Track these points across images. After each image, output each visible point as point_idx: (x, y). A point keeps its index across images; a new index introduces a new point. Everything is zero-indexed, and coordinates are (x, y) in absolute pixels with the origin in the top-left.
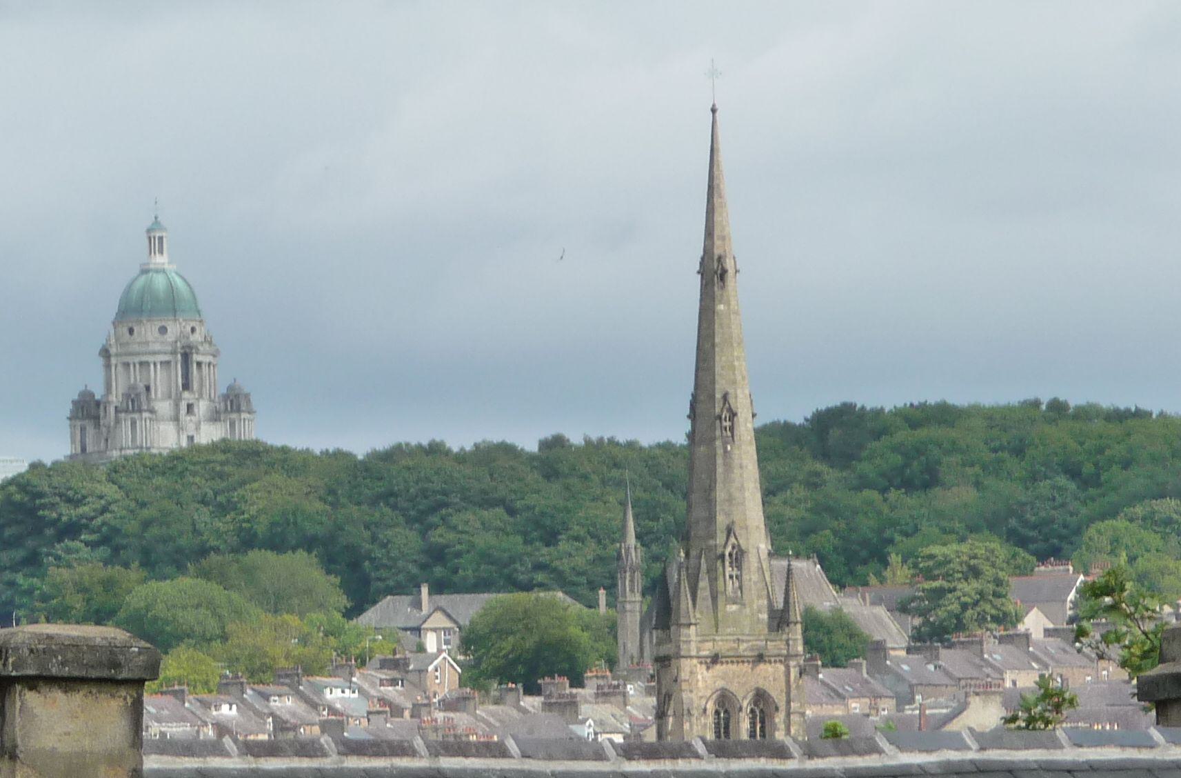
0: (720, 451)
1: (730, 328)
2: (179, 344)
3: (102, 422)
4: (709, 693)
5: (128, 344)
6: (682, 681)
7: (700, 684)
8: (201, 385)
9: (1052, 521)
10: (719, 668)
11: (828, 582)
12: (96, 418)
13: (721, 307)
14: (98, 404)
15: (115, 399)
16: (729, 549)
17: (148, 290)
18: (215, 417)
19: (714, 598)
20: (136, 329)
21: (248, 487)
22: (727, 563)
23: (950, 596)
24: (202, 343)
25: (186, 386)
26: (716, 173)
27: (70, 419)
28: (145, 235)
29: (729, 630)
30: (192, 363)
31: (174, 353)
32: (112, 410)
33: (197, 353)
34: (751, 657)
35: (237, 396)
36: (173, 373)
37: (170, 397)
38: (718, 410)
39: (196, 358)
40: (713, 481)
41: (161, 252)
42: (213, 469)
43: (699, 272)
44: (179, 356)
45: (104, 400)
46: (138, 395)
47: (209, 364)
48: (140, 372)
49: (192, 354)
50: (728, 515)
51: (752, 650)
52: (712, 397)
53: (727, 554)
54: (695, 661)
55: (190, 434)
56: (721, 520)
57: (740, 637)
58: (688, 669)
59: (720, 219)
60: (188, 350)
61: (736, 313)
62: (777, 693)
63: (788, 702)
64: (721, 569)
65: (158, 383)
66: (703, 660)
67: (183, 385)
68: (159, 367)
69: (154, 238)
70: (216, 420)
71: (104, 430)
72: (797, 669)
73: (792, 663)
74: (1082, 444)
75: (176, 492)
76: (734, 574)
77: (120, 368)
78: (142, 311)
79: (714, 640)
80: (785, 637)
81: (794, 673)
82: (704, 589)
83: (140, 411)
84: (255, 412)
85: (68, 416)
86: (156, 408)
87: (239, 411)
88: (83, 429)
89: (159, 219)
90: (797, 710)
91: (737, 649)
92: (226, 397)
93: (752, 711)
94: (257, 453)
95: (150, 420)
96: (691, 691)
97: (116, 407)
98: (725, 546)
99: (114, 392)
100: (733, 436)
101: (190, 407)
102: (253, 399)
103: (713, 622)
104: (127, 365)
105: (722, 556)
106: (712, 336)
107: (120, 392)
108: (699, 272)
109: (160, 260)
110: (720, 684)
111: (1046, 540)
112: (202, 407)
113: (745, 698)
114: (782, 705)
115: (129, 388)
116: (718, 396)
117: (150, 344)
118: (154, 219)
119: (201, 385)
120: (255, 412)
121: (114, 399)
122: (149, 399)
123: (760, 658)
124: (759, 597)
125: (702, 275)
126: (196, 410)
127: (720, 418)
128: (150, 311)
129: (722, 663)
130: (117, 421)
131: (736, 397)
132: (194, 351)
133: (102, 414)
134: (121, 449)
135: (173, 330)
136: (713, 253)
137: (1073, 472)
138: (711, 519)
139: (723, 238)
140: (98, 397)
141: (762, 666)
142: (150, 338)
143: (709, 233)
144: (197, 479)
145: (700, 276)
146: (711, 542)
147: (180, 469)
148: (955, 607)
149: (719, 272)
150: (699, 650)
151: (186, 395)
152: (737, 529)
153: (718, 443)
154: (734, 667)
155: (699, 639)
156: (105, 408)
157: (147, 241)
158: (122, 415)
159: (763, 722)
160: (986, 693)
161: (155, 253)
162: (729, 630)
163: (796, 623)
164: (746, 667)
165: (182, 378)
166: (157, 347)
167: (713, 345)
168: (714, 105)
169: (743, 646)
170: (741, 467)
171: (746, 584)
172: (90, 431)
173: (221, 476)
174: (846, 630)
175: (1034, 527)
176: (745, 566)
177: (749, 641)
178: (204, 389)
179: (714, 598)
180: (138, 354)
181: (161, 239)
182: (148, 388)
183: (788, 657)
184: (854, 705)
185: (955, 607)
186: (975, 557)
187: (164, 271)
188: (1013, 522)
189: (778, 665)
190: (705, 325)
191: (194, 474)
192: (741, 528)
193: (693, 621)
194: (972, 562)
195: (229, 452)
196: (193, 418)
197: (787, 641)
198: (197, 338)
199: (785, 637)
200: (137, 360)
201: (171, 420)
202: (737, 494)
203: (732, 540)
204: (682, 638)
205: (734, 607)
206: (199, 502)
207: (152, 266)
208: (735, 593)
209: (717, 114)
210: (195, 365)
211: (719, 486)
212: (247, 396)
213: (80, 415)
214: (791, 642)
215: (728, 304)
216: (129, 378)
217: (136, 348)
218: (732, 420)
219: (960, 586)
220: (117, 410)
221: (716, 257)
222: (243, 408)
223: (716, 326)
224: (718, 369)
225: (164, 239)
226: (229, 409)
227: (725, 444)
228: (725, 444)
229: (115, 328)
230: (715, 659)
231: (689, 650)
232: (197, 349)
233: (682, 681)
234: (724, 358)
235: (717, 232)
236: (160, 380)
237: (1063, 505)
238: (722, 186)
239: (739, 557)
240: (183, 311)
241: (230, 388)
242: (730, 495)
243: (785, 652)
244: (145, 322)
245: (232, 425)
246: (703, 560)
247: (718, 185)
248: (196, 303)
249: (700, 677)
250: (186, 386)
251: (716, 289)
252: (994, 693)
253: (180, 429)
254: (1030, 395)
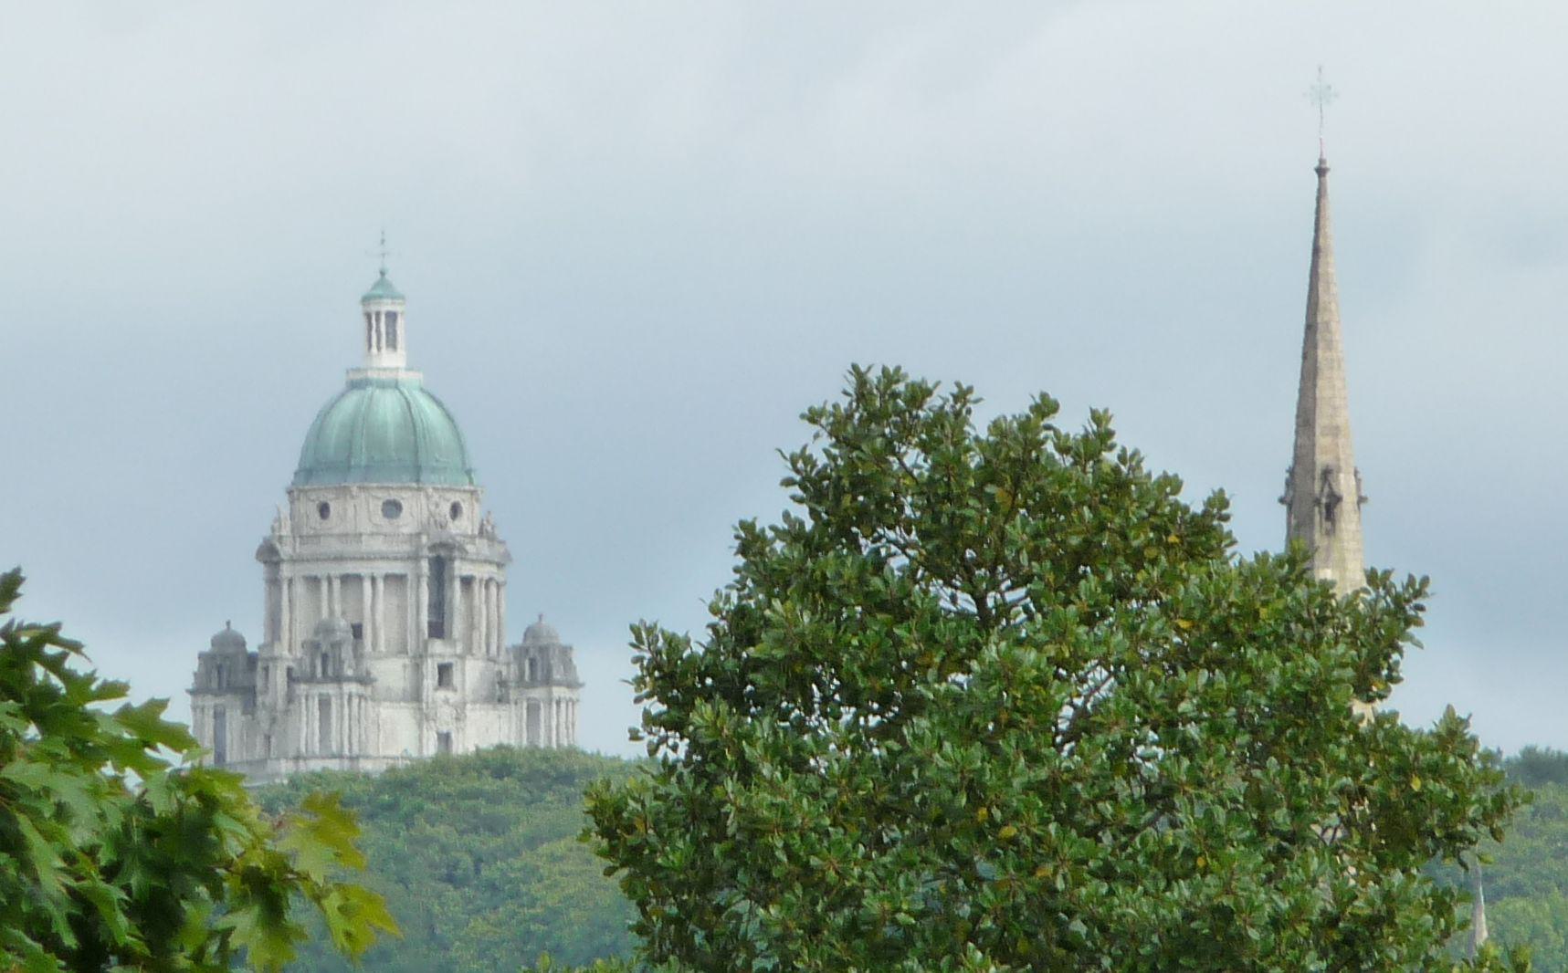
2: (424, 539)
3: (260, 699)
5: (317, 536)
8: (471, 627)
12: (248, 695)
14: (252, 660)
15: (288, 653)
17: (361, 424)
18: (498, 693)
20: (333, 506)
21: (544, 848)
24: (472, 537)
25: (438, 629)
26: (1323, 298)
27: (193, 692)
28: (360, 308)
30: (452, 579)
31: (415, 558)
32: (280, 678)
33: (463, 559)
35: (543, 650)
36: (411, 599)
37: (403, 651)
39: (461, 568)
41: (392, 344)
42: (475, 812)
43: (1282, 501)
44: (425, 565)
45: (265, 654)
46: (337, 645)
47: (488, 583)
48: (344, 600)
49: (452, 560)
55: (444, 729)
60: (443, 553)
65: (379, 617)
67: (431, 625)
68: (381, 585)
69: (378, 314)
70: (500, 701)
71: (262, 715)
75: (400, 859)
77: (300, 588)
78: (349, 468)
83: (339, 679)
84: (581, 685)
85: (190, 687)
86: (374, 673)
87: (548, 681)
88: (219, 715)
89: (387, 277)
92: (521, 652)
94: (567, 778)
95: (361, 697)
97: (289, 670)
99: (285, 636)
101: (444, 671)
102: (578, 659)
104: (314, 581)
107: (300, 637)
109: (390, 361)
112: (471, 673)
115: (317, 633)
117: (364, 538)
118: (379, 276)
119: (471, 627)
120: (581, 685)
121: (286, 653)
122: (358, 656)
125: (1290, 506)
126: (456, 678)
128: (367, 467)
130: (290, 698)
132: (456, 553)
133: (260, 683)
134: (297, 758)
135: (415, 509)
136: (1314, 463)
139: (1335, 431)
140: (252, 648)
142: (366, 528)
143: (1306, 420)
144: (441, 830)
145: (1284, 508)
147: (405, 808)
149: (1324, 500)
151: (438, 647)
156: (266, 669)
157: (363, 322)
158: (302, 688)
161: (379, 348)
165: (430, 613)
166: (377, 545)
168: (1322, 161)
172: (235, 718)
173: (494, 826)
178: (476, 635)
180: (340, 559)
181: (392, 317)
182: (357, 631)
187: (396, 385)
191: (432, 819)
195: (509, 774)
196: (450, 695)
198: (463, 527)
200: (337, 570)
201: (404, 699)
206: (441, 880)
207: (372, 375)
210: (457, 584)
212: (566, 651)
213: (214, 685)
216: (319, 609)
217: (335, 547)
220: (291, 678)
221: (1318, 472)
222: (557, 676)
225: (400, 322)
226: (527, 678)
229: (292, 502)
232: (462, 549)
235: (1321, 421)
236: (380, 610)
238: (1333, 326)
240: (434, 470)
241: (531, 633)
244: (355, 490)
245: (533, 709)
247: (1327, 324)
248: (462, 448)
250: (438, 629)
251: (1317, 536)
253: (423, 718)
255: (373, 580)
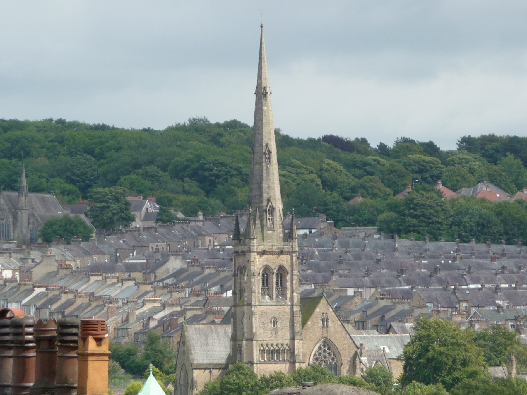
0: (265, 168)
1: (268, 117)
4: (261, 267)
6: (251, 262)
7: (257, 263)
10: (265, 257)
11: (365, 228)
13: (265, 108)
16: (268, 208)
19: (262, 228)
22: (268, 214)
23: (108, 210)
29: (268, 241)
34: (278, 252)
38: (264, 151)
40: (262, 180)
43: (255, 94)
51: (278, 249)
52: (261, 145)
53: (268, 209)
54: (256, 253)
56: (265, 196)
57: (274, 244)
58: (253, 257)
59: (264, 72)
61: (271, 111)
63: (292, 271)
64: (265, 216)
66: (259, 253)
72: (296, 257)
73: (294, 255)
74: (91, 140)
76: (270, 217)
79: (263, 245)
80: (291, 244)
81: (295, 259)
82: (258, 224)
90: (295, 274)
91: (272, 249)
93: (277, 274)
96: (254, 266)
98: (267, 207)
100: (270, 162)
103: (262, 238)
105: (266, 210)
108: (255, 94)
110: (265, 263)
111: (84, 181)
113: (275, 269)
114: (289, 271)
116: (264, 145)
123: (282, 253)
124: (280, 228)
127: (265, 153)
129: (266, 254)
131: (271, 145)
137: (90, 152)
138: (261, 195)
139: (266, 79)
141: (282, 256)
146: (261, 205)
148: (110, 214)
150: (257, 249)
152: (272, 200)
153: (264, 164)
154: (271, 256)
155: (258, 244)
159: (281, 278)
160: (176, 255)
162: (268, 241)
163: (296, 238)
167: (262, 124)
169: (275, 248)
170: (273, 174)
171: (275, 222)
174: (83, 225)
175: (78, 176)
176: (275, 214)
177: (277, 245)
179: (262, 228)
184: (95, 258)
185: (110, 214)
186: (117, 193)
188: (69, 174)
189: (288, 255)
190: (258, 115)
192: (273, 199)
193: (256, 237)
194: (117, 195)
197: (292, 245)
199: (291, 244)
202: (271, 185)
203: (270, 204)
204: (251, 244)
205: (270, 232)
208: (270, 226)
209: (263, 28)
211: (264, 182)
214: (294, 246)
215: (268, 107)
218: (269, 154)
219: (111, 206)
221: (263, 87)
223: (263, 116)
224: (264, 134)
227: (267, 164)
228: (267, 164)
230: (264, 253)
231: (254, 249)
233: (251, 262)
234: (266, 129)
235: (263, 77)
237: (90, 167)
239: (272, 211)
242: (269, 186)
243: (291, 250)
246: (257, 212)
249: (257, 260)
251: (263, 101)
252: (179, 255)
254: (48, 117)
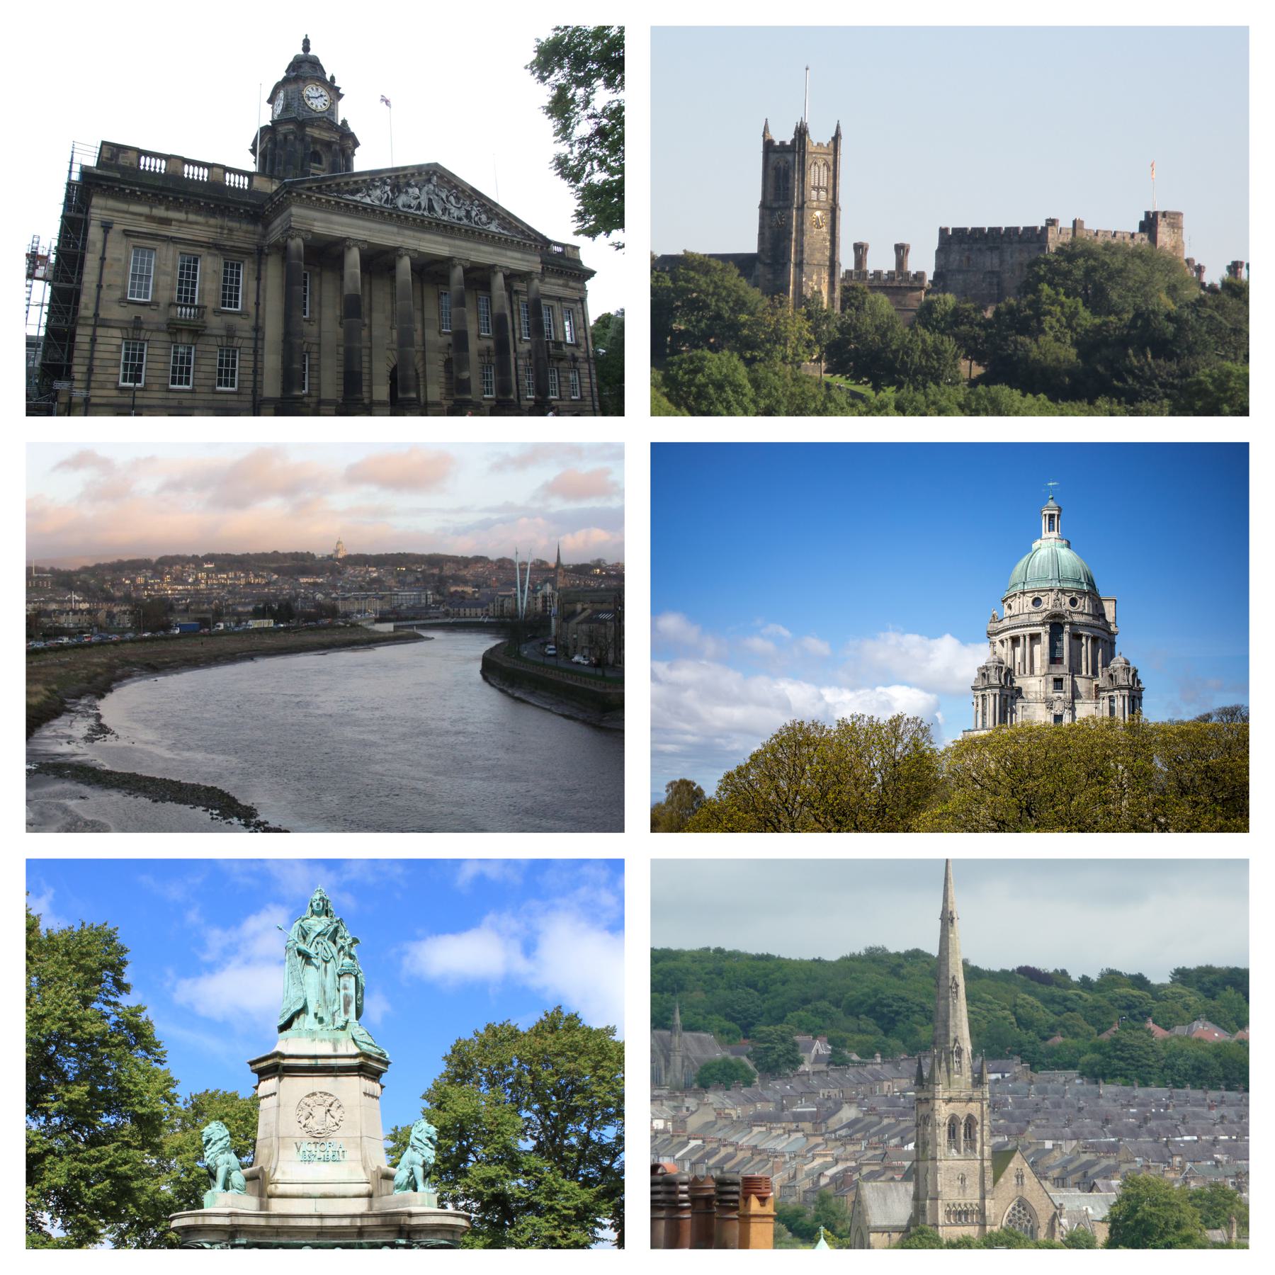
0: (951, 1003)
9: (748, 1010)
13: (951, 935)
19: (948, 1071)
40: (948, 1017)
50: (955, 1033)
56: (952, 1035)
62: (977, 1117)
63: (982, 1120)
81: (985, 1107)
106: (947, 949)
110: (952, 1111)
111: (745, 1018)
114: (979, 1121)
123: (971, 1100)
138: (947, 1035)
148: (775, 1056)
164: (964, 1104)
179: (948, 1071)
183: (984, 1099)
185: (775, 1056)
188: (728, 1010)
230: (950, 1100)
235: (950, 900)
239: (960, 1052)
254: (705, 945)
255: (1024, 636)
